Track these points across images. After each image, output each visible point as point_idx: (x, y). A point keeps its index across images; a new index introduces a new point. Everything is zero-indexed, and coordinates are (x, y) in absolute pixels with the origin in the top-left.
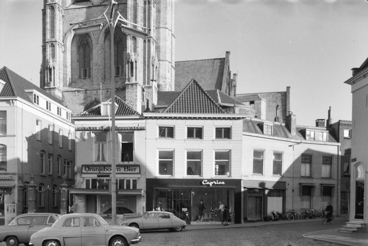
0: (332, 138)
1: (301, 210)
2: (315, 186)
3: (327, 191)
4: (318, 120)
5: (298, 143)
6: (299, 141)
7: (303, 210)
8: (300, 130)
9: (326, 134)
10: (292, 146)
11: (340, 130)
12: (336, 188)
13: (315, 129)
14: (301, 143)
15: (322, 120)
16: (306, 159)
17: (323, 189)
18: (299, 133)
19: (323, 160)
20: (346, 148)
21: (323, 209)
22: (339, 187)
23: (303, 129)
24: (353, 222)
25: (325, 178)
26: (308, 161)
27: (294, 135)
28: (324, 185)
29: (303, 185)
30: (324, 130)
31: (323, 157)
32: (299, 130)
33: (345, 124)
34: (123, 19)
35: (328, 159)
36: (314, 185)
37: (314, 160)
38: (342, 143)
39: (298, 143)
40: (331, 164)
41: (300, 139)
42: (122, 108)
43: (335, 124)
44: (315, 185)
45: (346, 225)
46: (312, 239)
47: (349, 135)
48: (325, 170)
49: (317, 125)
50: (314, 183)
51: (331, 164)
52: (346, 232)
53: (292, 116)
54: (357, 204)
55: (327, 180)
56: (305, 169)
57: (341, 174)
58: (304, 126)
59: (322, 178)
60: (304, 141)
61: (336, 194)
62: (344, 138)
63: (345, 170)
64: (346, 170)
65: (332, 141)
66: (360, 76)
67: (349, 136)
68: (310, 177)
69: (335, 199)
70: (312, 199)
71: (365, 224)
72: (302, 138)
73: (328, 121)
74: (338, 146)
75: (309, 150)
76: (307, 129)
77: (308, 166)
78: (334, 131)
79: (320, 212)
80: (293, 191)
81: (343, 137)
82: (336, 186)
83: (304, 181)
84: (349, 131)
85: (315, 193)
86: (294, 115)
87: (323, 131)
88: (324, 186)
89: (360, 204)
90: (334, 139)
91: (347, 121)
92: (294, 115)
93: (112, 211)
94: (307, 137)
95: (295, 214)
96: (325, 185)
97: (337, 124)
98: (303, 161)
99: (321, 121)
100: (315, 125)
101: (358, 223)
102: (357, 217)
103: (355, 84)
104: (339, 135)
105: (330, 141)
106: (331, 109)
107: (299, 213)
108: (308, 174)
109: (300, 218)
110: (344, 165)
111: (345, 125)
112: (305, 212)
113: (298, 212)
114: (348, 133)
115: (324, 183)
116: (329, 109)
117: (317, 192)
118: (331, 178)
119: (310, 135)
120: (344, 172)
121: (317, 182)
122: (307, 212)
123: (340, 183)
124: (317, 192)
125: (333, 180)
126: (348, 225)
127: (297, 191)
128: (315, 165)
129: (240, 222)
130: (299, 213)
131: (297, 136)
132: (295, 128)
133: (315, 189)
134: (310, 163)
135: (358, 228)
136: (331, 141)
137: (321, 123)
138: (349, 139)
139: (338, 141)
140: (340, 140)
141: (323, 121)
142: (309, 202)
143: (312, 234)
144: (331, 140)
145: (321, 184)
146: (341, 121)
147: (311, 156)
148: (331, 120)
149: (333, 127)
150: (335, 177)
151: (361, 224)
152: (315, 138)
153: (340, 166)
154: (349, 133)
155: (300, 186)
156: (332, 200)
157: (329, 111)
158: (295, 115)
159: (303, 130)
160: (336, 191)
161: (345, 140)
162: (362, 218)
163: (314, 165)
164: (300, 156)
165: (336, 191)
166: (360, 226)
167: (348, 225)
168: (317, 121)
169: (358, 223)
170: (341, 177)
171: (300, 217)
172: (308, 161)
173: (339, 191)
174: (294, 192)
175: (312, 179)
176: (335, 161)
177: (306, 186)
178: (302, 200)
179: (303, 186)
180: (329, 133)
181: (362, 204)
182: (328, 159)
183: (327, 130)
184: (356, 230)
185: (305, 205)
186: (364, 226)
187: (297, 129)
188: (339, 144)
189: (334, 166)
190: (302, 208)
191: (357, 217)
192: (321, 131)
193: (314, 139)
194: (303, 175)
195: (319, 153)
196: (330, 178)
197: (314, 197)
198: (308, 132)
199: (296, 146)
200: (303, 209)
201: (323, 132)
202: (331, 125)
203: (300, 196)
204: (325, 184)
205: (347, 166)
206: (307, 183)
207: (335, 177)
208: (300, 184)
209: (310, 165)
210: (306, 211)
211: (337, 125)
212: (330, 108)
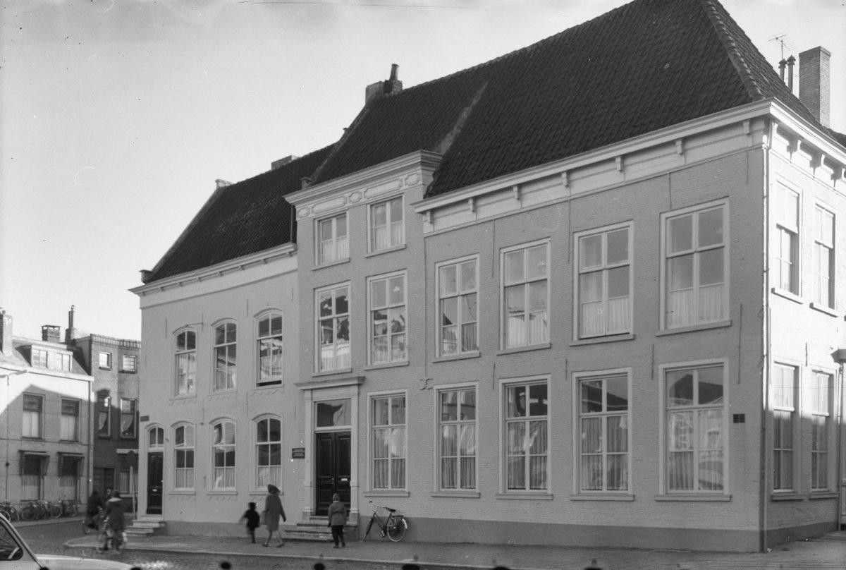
0: (77, 365)
1: (23, 503)
2: (49, 456)
3: (70, 466)
4: (46, 326)
5: (19, 372)
6: (21, 369)
7: (27, 503)
8: (20, 345)
9: (68, 356)
10: (6, 377)
11: (93, 353)
12: (86, 461)
13: (39, 345)
14: (25, 372)
15: (54, 327)
16: (32, 403)
17: (62, 462)
18: (18, 353)
19: (62, 407)
20: (102, 386)
21: (63, 501)
22: (91, 459)
23: (24, 344)
24: (144, 519)
25: (66, 441)
26: (35, 407)
27: (7, 355)
28: (65, 455)
29: (26, 453)
30: (63, 349)
31: (64, 401)
32: (18, 346)
33: (100, 342)
34: (461, 432)
35: (71, 405)
36: (46, 454)
37: (47, 406)
38: (95, 377)
39: (19, 372)
40: (76, 414)
41: (21, 364)
42: (581, 478)
43: (82, 340)
44: (49, 454)
45: (132, 525)
46: (90, 548)
47: (108, 362)
48: (66, 426)
49: (45, 338)
50: (47, 450)
51: (76, 414)
52: (135, 535)
53: (5, 318)
54: (149, 491)
55: (71, 445)
56: (29, 424)
57: (95, 435)
58: (26, 339)
59: (62, 441)
60: (29, 369)
61: (85, 471)
62: (100, 368)
63: (100, 428)
64: (104, 427)
65: (79, 373)
66: (174, 282)
67: (108, 365)
68: (39, 439)
69: (83, 480)
70: (42, 480)
71: (165, 522)
72: (26, 364)
73: (69, 332)
74: (89, 382)
75: (32, 387)
76: (33, 346)
77: (35, 416)
78: (81, 353)
79: (56, 506)
80: (7, 465)
81: (98, 366)
82: (86, 456)
83: (27, 447)
84: (108, 355)
85: (48, 471)
86: (10, 317)
87: (62, 352)
88: (65, 457)
89: (155, 490)
90: (81, 369)
91: (104, 337)
92: (8, 316)
93: (697, 466)
94: (33, 361)
95: (12, 511)
96: (67, 455)
97: (85, 341)
98: (26, 407)
99: (52, 328)
100: (41, 335)
101: (154, 521)
102: (150, 511)
103: (163, 292)
104: (90, 362)
105: (75, 371)
106: (74, 310)
107: (18, 508)
108: (35, 433)
109: (21, 519)
110: (98, 417)
111: (102, 343)
112: (29, 506)
113: (16, 507)
114: (106, 360)
115: (65, 451)
116: (70, 310)
117: (52, 468)
118: (77, 441)
119: (37, 358)
120: (100, 431)
121: (51, 449)
122: (35, 506)
123: (92, 451)
124: (52, 468)
125: (80, 446)
126: (135, 525)
127: (14, 466)
128: (48, 415)
129: (384, 485)
130: (18, 508)
131: (15, 358)
132: (11, 341)
133: (49, 461)
134: (39, 410)
135: (155, 529)
136: (76, 371)
137: (52, 333)
138: (109, 370)
139: (89, 373)
140: (94, 370)
141: (57, 329)
142: (73, 488)
143: (88, 541)
144: (77, 369)
145: (60, 453)
146: (95, 336)
147: (42, 398)
148: (75, 331)
149: (78, 345)
150: (84, 440)
151: (160, 523)
152: (48, 364)
153: (92, 419)
154: (108, 358)
155: (21, 457)
156: (42, 483)
157: (71, 314)
158: (11, 317)
159: (24, 346)
160: (86, 465)
161: (102, 371)
162: (159, 512)
163: (47, 417)
164: (18, 398)
165: (86, 465)
166: (157, 525)
167: (135, 525)
168: (45, 328)
169: (154, 521)
170: (94, 439)
171: (20, 516)
172: (35, 407)
173: (91, 466)
174: (9, 467)
175: (43, 443)
176: (83, 410)
177: (31, 455)
178: (24, 484)
179: (27, 456)
180: (74, 356)
181: (160, 491)
182: (71, 406)
183: (68, 350)
184: (151, 531)
185: (30, 493)
186: (163, 525)
187: (14, 343)
188: (91, 379)
189: (83, 419)
190: (23, 499)
191: (150, 511)
192: (58, 351)
193: (47, 366)
194: (26, 434)
195: (57, 395)
196: (75, 441)
197: (45, 477)
198: (34, 352)
199: (13, 377)
200: (25, 501)
201: (62, 355)
202: (74, 340)
203: (21, 475)
204: (66, 453)
205: (104, 421)
206: (33, 450)
207: (84, 440)
208: (21, 452)
209: (76, 421)
210: (31, 504)
211: (88, 342)
212: (72, 309)
